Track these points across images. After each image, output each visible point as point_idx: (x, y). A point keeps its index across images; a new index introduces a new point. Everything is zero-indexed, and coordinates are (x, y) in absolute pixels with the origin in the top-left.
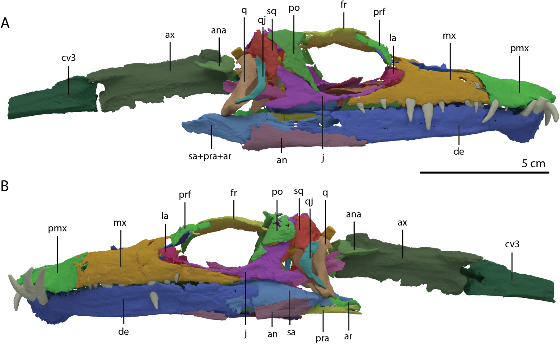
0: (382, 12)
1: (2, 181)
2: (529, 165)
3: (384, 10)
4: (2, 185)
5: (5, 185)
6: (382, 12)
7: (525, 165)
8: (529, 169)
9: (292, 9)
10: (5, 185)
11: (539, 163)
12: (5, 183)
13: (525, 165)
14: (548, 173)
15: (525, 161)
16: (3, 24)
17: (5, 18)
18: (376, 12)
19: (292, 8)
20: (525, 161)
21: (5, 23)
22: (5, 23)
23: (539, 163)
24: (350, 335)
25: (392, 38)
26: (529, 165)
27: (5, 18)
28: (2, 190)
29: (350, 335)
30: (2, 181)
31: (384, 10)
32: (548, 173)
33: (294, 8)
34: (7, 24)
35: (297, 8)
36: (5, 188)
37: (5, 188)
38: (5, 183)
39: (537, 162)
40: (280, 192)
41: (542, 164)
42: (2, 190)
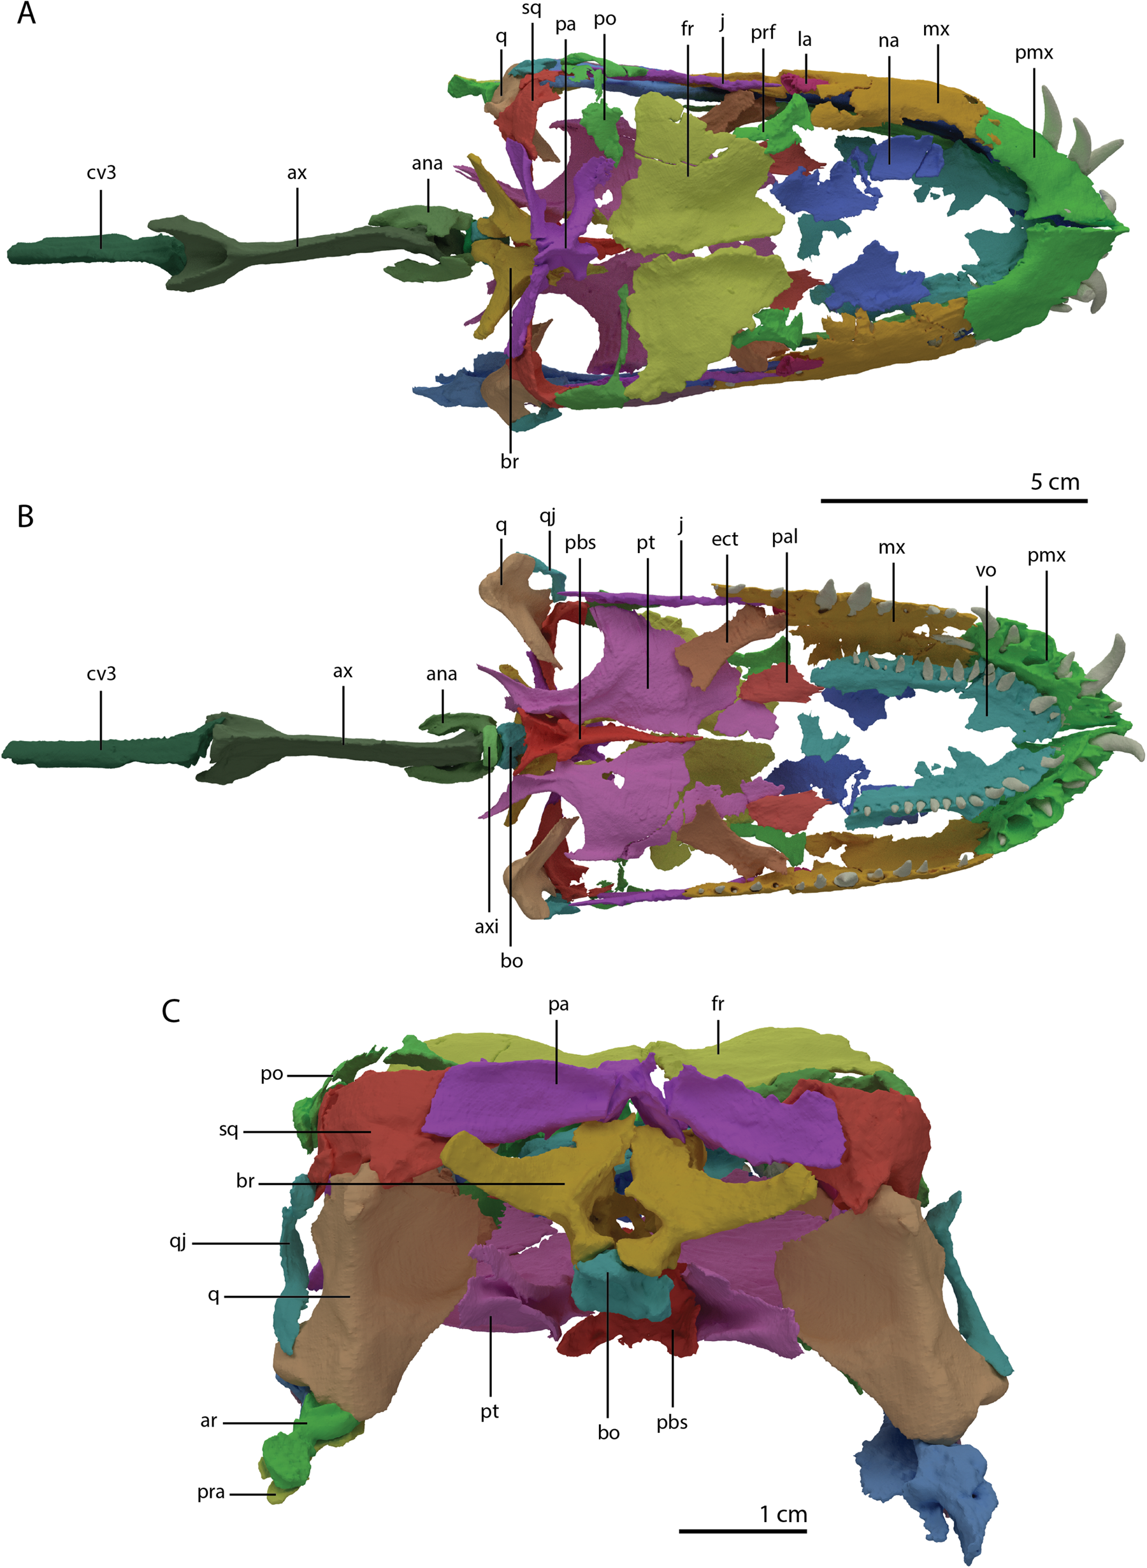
0: (768, 33)
1: (21, 507)
2: (1045, 484)
3: (772, 29)
4: (21, 515)
5: (27, 515)
6: (768, 33)
7: (1036, 485)
8: (1045, 493)
9: (600, 20)
10: (27, 515)
11: (794, 1514)
12: (25, 511)
13: (1036, 485)
14: (1085, 501)
15: (1037, 477)
16: (22, 15)
17: (27, 3)
18: (757, 34)
19: (600, 20)
20: (1037, 477)
21: (26, 12)
22: (26, 12)
23: (794, 1514)
24: (251, 1179)
25: (803, 39)
26: (1045, 484)
27: (27, 3)
28: (21, 525)
29: (251, 1179)
30: (21, 507)
31: (772, 29)
32: (1085, 501)
33: (605, 20)
34: (31, 15)
35: (611, 20)
36: (26, 521)
37: (26, 521)
38: (25, 511)
39: (791, 1512)
40: (518, 962)
41: (802, 1515)
42: (21, 525)
